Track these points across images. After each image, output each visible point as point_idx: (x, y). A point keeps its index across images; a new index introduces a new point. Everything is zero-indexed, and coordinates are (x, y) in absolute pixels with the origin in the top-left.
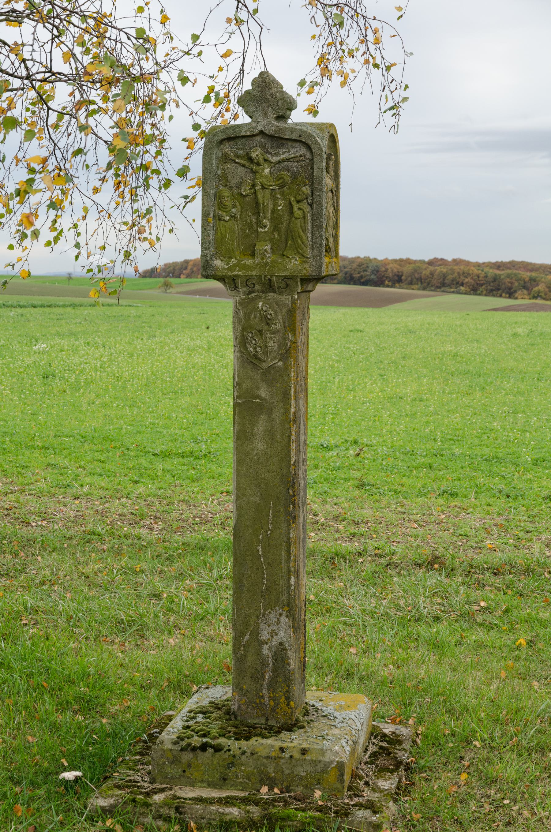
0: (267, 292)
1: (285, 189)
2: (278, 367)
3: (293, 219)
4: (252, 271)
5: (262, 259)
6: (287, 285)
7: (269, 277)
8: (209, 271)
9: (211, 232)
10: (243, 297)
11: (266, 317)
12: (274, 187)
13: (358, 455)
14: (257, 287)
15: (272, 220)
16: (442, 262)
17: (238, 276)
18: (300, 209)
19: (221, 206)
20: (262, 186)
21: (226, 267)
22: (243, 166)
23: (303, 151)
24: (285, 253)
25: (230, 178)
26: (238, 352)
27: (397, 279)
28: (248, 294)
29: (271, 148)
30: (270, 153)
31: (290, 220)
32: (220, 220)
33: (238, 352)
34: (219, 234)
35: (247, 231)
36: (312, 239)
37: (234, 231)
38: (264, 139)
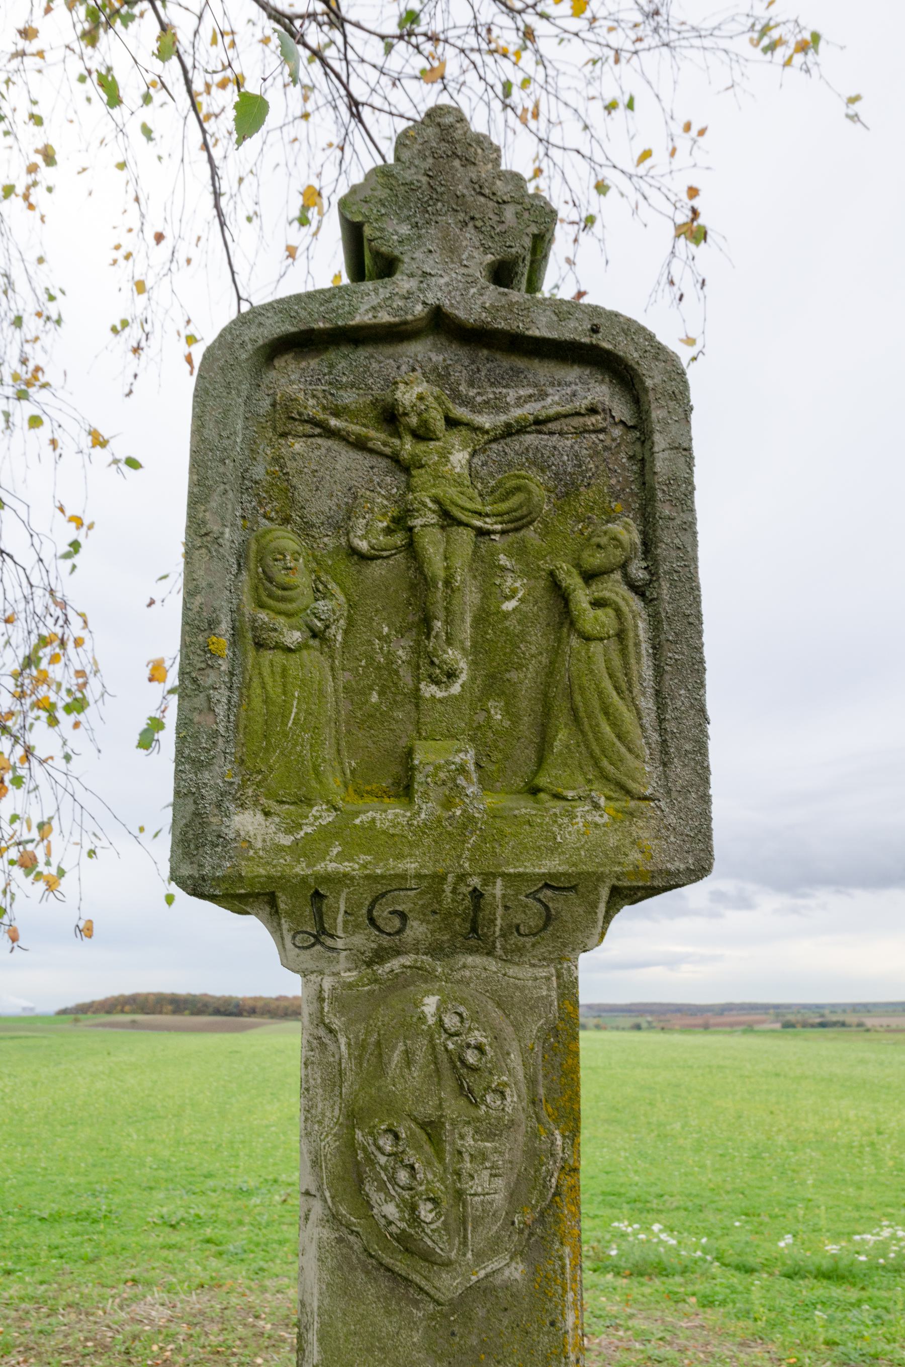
0: (454, 952)
1: (530, 534)
2: (506, 1286)
3: (575, 641)
4: (400, 857)
5: (448, 804)
6: (549, 918)
7: (475, 881)
8: (208, 862)
9: (221, 695)
10: (350, 976)
11: (457, 1062)
12: (488, 524)
13: (285, 1201)
14: (417, 930)
15: (479, 651)
16: (285, 998)
17: (338, 880)
18: (598, 604)
19: (270, 589)
20: (445, 514)
21: (286, 840)
22: (360, 445)
23: (599, 391)
24: (542, 781)
25: (303, 492)
26: (322, 1222)
27: (253, 1012)
28: (369, 964)
29: (471, 384)
30: (466, 402)
31: (556, 652)
32: (260, 645)
33: (322, 1222)
34: (257, 703)
35: (374, 698)
36: (661, 721)
37: (322, 693)
38: (439, 351)
